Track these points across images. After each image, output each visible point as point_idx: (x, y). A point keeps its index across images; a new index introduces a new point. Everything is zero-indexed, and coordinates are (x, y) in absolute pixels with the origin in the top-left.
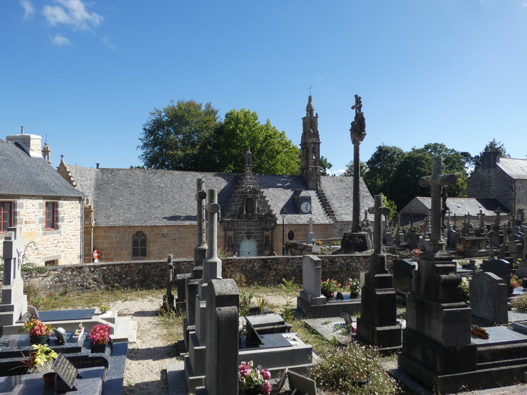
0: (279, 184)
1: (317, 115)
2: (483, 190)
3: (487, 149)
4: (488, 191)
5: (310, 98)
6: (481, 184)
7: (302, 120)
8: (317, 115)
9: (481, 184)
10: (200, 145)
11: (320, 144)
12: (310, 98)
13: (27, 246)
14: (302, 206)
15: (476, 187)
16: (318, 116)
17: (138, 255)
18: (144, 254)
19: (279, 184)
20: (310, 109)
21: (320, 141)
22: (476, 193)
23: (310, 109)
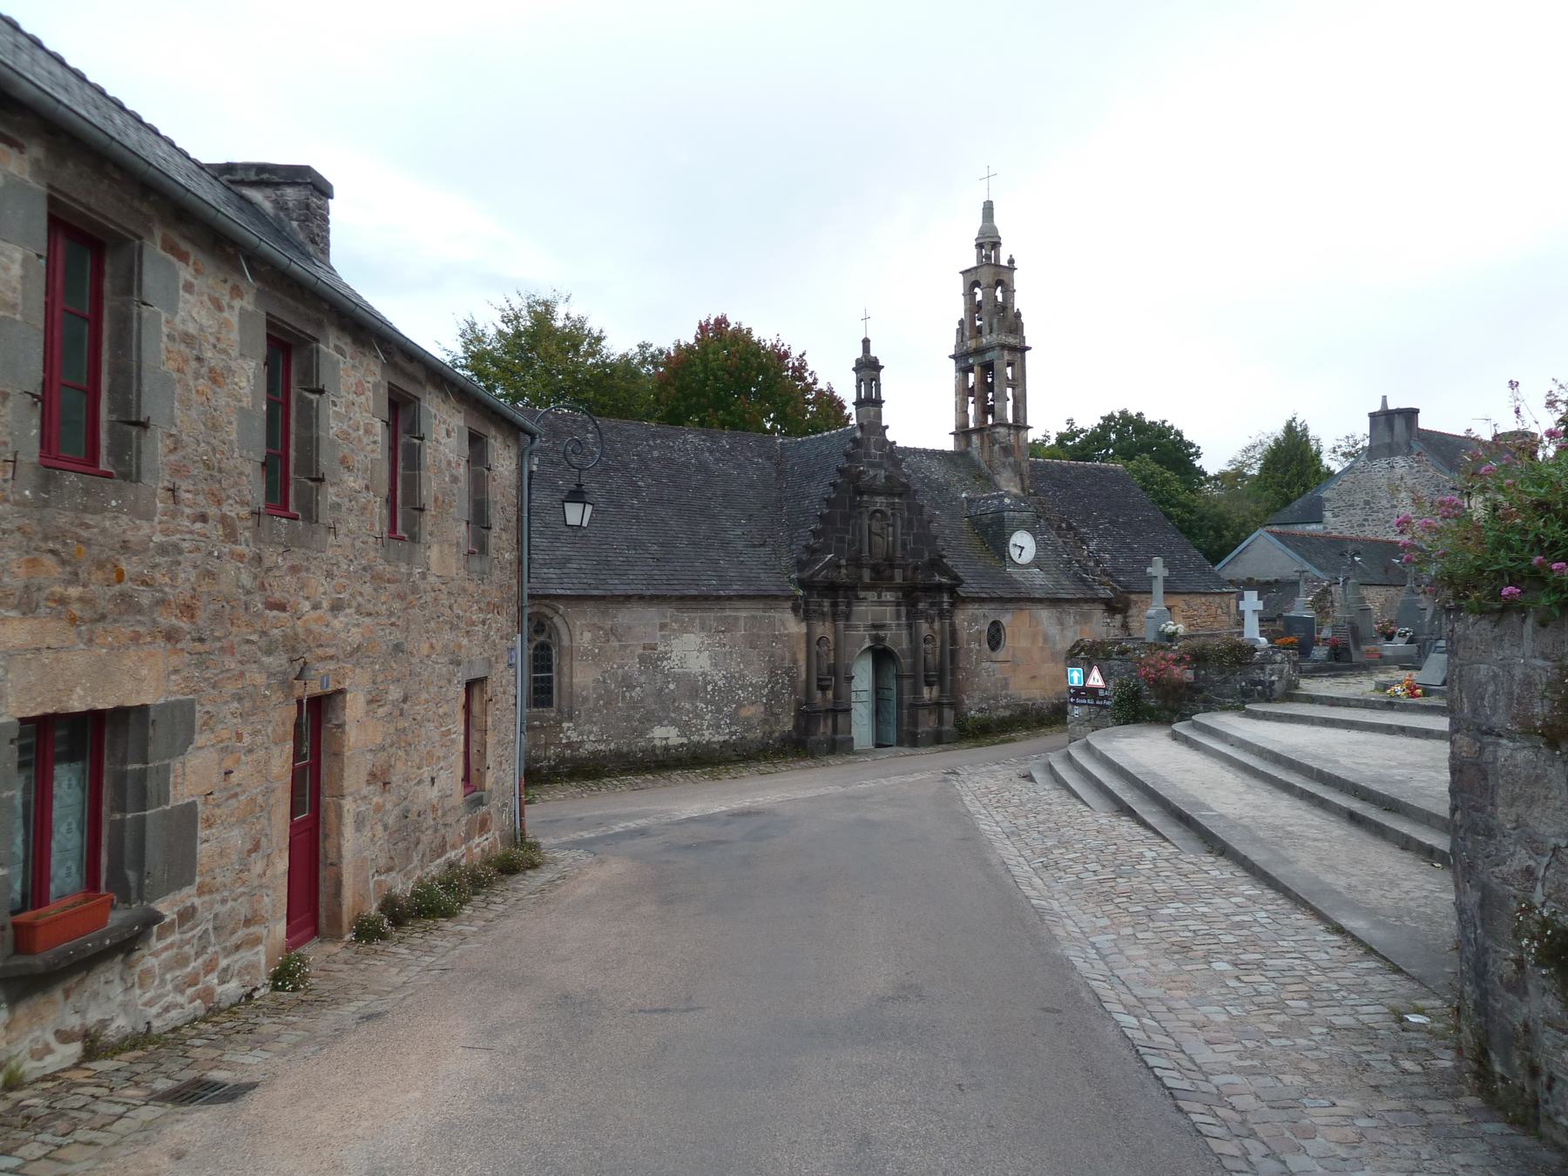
0: (971, 409)
1: (1011, 261)
2: (1373, 520)
3: (1191, 445)
4: (1387, 522)
5: (988, 209)
6: (1367, 502)
7: (953, 361)
8: (1011, 261)
9: (1367, 502)
10: (1494, 1082)
11: (1027, 353)
12: (988, 209)
13: (235, 621)
14: (1033, 551)
15: (1352, 511)
16: (1016, 265)
17: (535, 693)
18: (30, 952)
19: (971, 409)
20: (988, 242)
21: (1027, 344)
22: (1352, 527)
23: (988, 242)
